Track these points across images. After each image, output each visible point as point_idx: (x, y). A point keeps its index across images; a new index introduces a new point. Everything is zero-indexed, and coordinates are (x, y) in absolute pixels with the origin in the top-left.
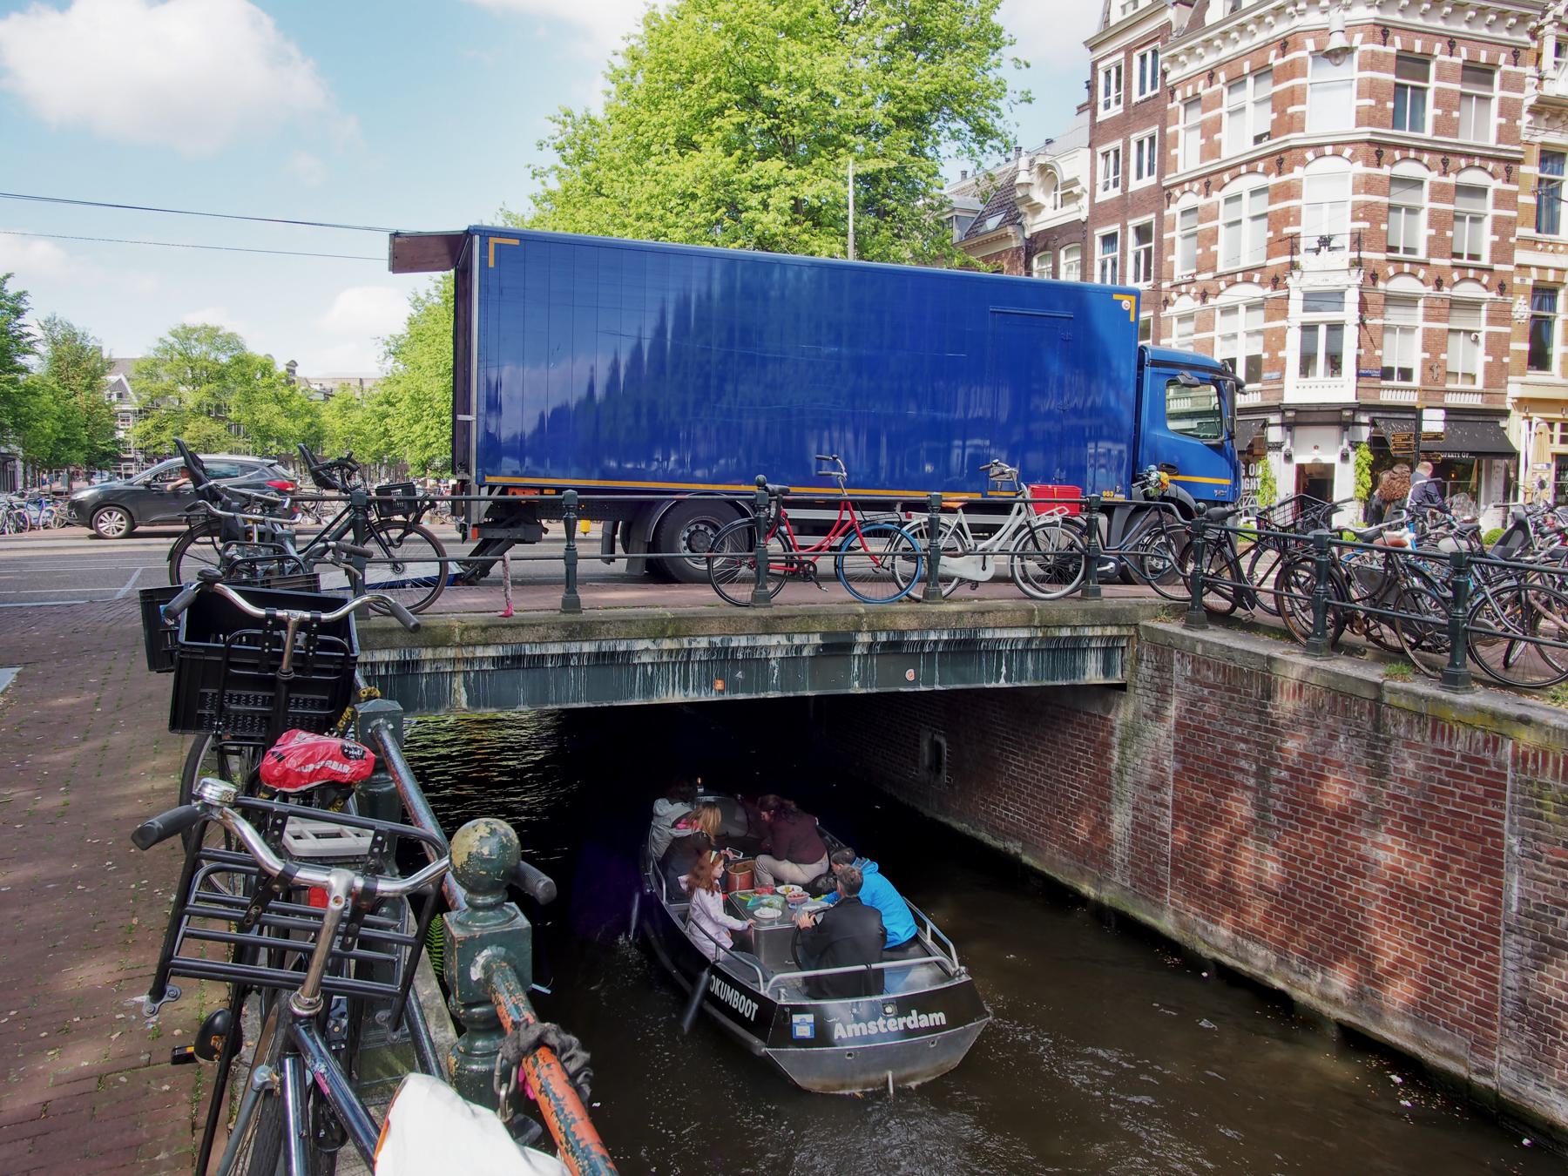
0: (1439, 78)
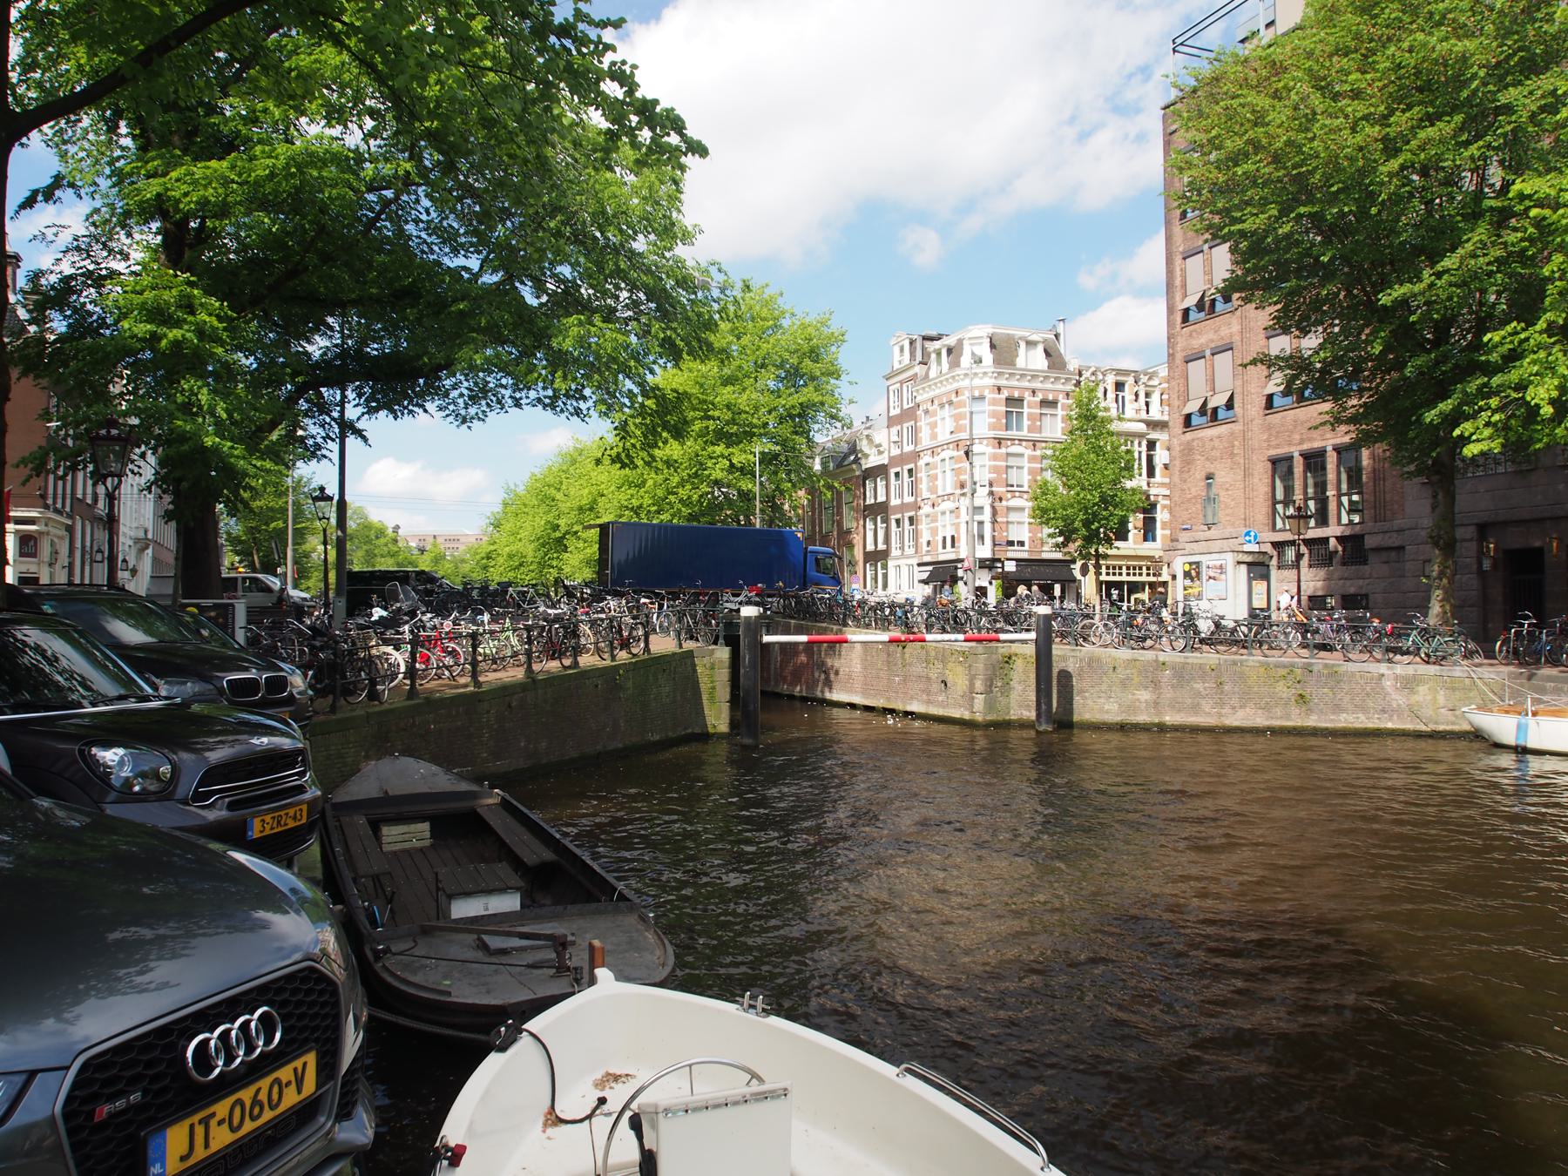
0: (1029, 407)
